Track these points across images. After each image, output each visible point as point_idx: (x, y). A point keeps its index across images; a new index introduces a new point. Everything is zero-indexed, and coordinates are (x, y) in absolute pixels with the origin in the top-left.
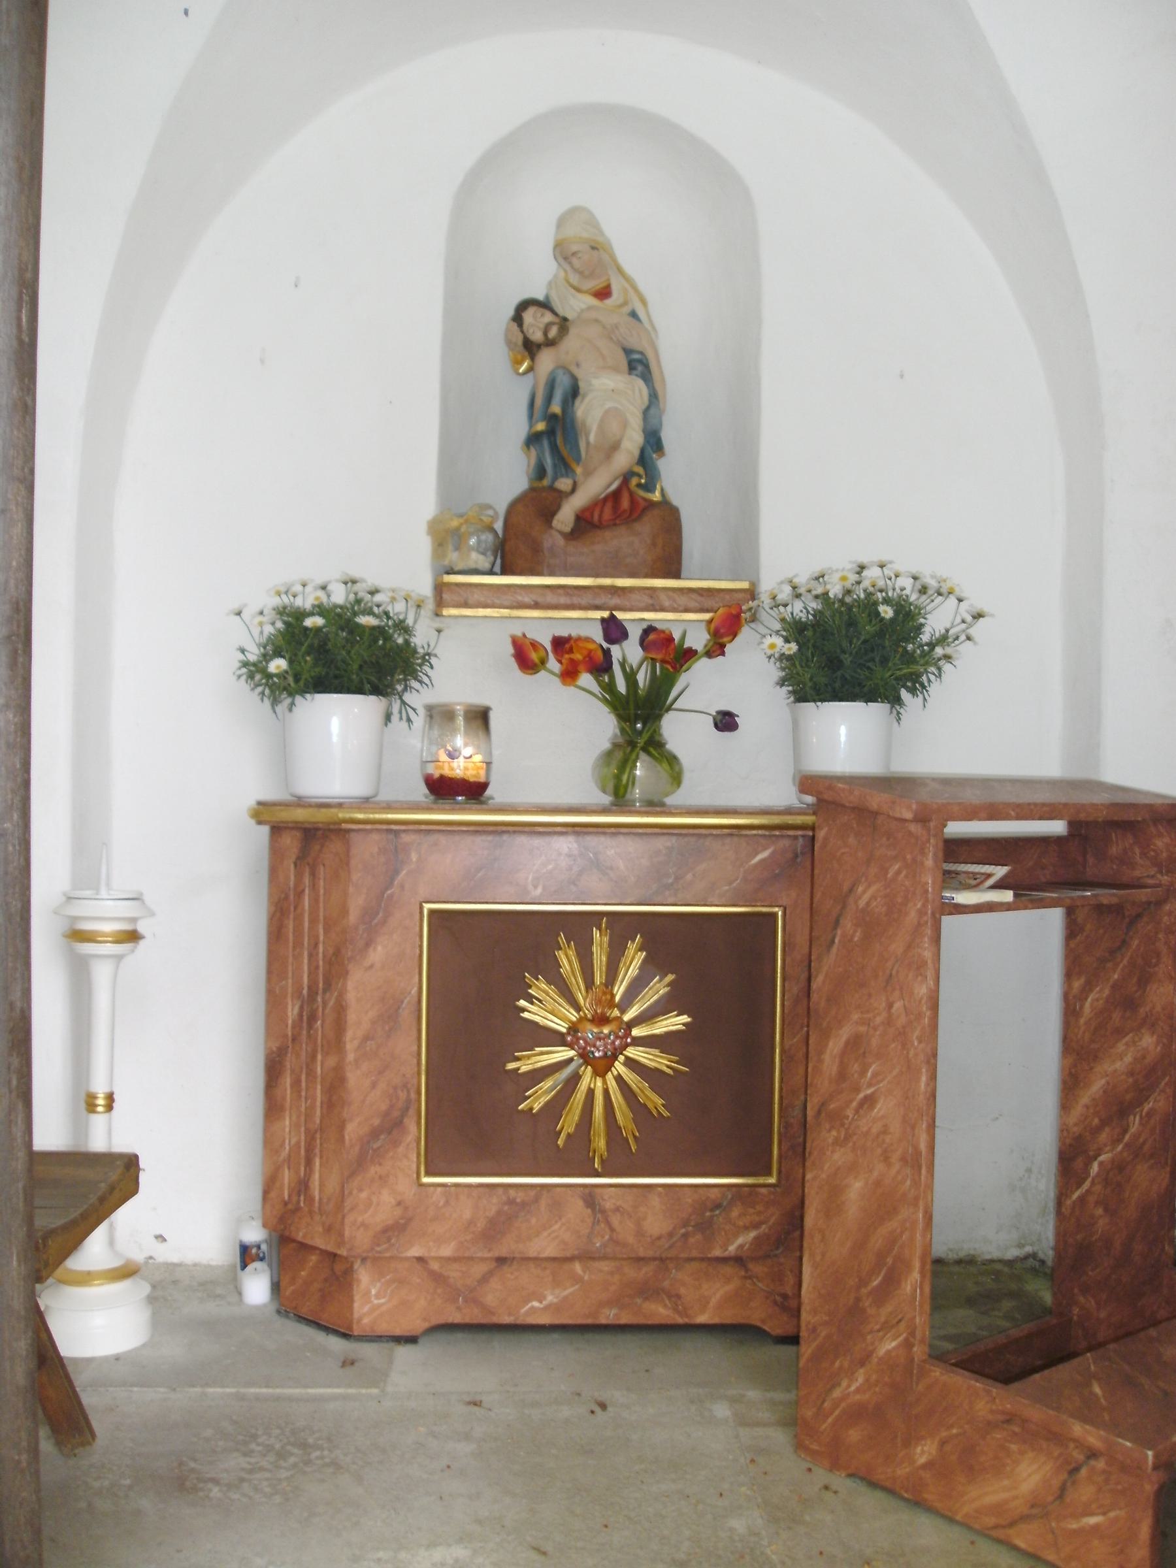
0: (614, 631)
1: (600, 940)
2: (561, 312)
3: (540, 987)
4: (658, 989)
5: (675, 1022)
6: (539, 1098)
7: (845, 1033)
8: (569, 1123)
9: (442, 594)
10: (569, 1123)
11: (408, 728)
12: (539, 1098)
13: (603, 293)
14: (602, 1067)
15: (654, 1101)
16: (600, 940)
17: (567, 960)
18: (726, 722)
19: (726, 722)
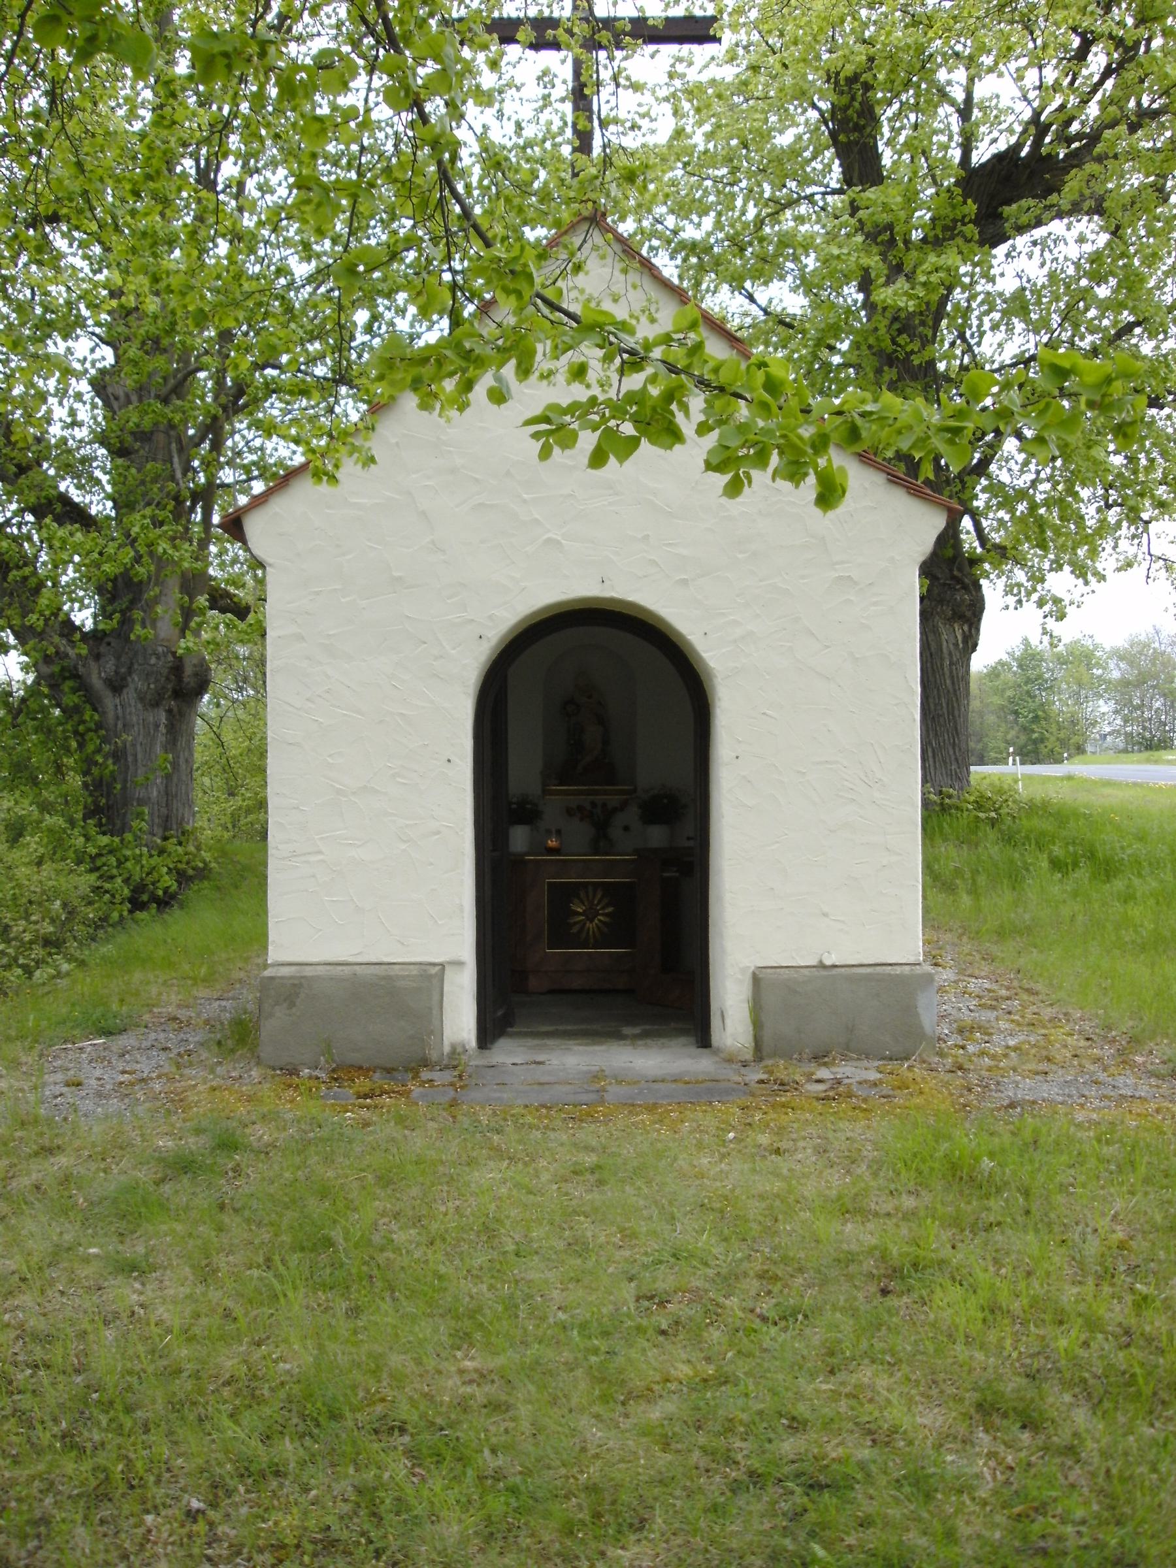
0: (594, 804)
1: (590, 889)
2: (256, 552)
3: (576, 901)
4: (605, 901)
5: (610, 909)
6: (575, 930)
7: (826, 1226)
8: (584, 935)
9: (545, 792)
10: (584, 935)
11: (529, 415)
12: (575, 930)
13: (590, 697)
14: (592, 921)
15: (606, 930)
16: (590, 889)
17: (582, 894)
18: (626, 828)
19: (626, 828)
